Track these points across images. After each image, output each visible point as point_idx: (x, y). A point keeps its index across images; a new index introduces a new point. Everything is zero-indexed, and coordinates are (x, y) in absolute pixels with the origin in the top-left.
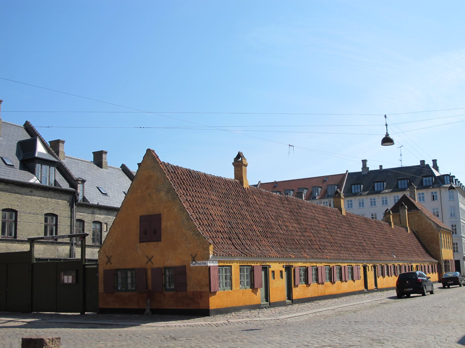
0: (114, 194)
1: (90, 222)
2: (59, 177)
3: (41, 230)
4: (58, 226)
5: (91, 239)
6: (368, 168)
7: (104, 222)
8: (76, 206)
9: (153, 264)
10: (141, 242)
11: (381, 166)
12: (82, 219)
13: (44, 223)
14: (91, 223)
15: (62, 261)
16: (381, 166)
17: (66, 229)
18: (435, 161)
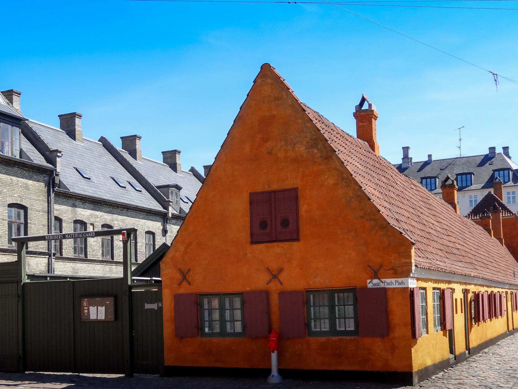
0: (99, 180)
1: (70, 221)
2: (25, 145)
3: (3, 230)
4: (29, 225)
5: (71, 248)
6: (411, 158)
7: (90, 222)
8: (53, 194)
9: (281, 284)
10: (253, 242)
11: (430, 156)
12: (58, 216)
13: (7, 218)
14: (71, 222)
15: (68, 279)
16: (430, 156)
17: (41, 231)
18: (506, 149)
